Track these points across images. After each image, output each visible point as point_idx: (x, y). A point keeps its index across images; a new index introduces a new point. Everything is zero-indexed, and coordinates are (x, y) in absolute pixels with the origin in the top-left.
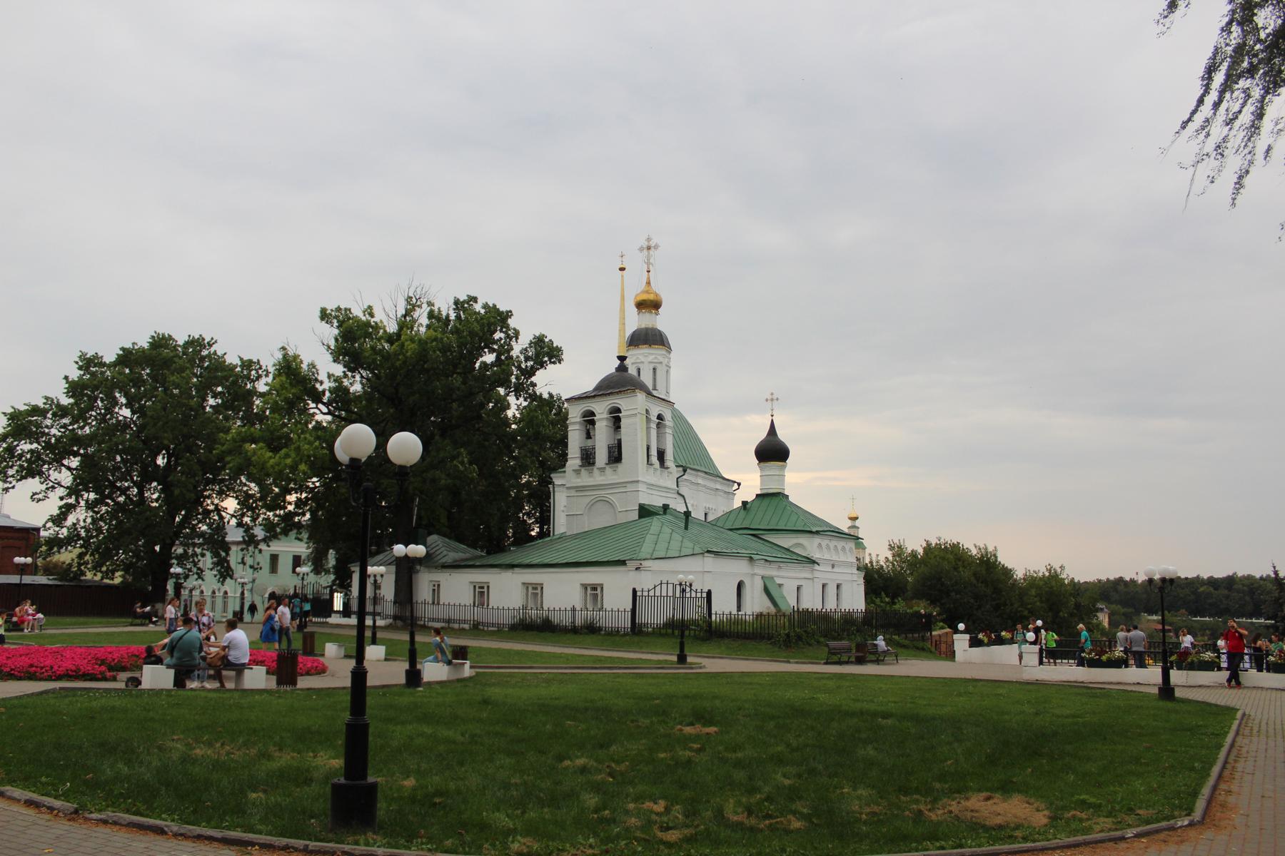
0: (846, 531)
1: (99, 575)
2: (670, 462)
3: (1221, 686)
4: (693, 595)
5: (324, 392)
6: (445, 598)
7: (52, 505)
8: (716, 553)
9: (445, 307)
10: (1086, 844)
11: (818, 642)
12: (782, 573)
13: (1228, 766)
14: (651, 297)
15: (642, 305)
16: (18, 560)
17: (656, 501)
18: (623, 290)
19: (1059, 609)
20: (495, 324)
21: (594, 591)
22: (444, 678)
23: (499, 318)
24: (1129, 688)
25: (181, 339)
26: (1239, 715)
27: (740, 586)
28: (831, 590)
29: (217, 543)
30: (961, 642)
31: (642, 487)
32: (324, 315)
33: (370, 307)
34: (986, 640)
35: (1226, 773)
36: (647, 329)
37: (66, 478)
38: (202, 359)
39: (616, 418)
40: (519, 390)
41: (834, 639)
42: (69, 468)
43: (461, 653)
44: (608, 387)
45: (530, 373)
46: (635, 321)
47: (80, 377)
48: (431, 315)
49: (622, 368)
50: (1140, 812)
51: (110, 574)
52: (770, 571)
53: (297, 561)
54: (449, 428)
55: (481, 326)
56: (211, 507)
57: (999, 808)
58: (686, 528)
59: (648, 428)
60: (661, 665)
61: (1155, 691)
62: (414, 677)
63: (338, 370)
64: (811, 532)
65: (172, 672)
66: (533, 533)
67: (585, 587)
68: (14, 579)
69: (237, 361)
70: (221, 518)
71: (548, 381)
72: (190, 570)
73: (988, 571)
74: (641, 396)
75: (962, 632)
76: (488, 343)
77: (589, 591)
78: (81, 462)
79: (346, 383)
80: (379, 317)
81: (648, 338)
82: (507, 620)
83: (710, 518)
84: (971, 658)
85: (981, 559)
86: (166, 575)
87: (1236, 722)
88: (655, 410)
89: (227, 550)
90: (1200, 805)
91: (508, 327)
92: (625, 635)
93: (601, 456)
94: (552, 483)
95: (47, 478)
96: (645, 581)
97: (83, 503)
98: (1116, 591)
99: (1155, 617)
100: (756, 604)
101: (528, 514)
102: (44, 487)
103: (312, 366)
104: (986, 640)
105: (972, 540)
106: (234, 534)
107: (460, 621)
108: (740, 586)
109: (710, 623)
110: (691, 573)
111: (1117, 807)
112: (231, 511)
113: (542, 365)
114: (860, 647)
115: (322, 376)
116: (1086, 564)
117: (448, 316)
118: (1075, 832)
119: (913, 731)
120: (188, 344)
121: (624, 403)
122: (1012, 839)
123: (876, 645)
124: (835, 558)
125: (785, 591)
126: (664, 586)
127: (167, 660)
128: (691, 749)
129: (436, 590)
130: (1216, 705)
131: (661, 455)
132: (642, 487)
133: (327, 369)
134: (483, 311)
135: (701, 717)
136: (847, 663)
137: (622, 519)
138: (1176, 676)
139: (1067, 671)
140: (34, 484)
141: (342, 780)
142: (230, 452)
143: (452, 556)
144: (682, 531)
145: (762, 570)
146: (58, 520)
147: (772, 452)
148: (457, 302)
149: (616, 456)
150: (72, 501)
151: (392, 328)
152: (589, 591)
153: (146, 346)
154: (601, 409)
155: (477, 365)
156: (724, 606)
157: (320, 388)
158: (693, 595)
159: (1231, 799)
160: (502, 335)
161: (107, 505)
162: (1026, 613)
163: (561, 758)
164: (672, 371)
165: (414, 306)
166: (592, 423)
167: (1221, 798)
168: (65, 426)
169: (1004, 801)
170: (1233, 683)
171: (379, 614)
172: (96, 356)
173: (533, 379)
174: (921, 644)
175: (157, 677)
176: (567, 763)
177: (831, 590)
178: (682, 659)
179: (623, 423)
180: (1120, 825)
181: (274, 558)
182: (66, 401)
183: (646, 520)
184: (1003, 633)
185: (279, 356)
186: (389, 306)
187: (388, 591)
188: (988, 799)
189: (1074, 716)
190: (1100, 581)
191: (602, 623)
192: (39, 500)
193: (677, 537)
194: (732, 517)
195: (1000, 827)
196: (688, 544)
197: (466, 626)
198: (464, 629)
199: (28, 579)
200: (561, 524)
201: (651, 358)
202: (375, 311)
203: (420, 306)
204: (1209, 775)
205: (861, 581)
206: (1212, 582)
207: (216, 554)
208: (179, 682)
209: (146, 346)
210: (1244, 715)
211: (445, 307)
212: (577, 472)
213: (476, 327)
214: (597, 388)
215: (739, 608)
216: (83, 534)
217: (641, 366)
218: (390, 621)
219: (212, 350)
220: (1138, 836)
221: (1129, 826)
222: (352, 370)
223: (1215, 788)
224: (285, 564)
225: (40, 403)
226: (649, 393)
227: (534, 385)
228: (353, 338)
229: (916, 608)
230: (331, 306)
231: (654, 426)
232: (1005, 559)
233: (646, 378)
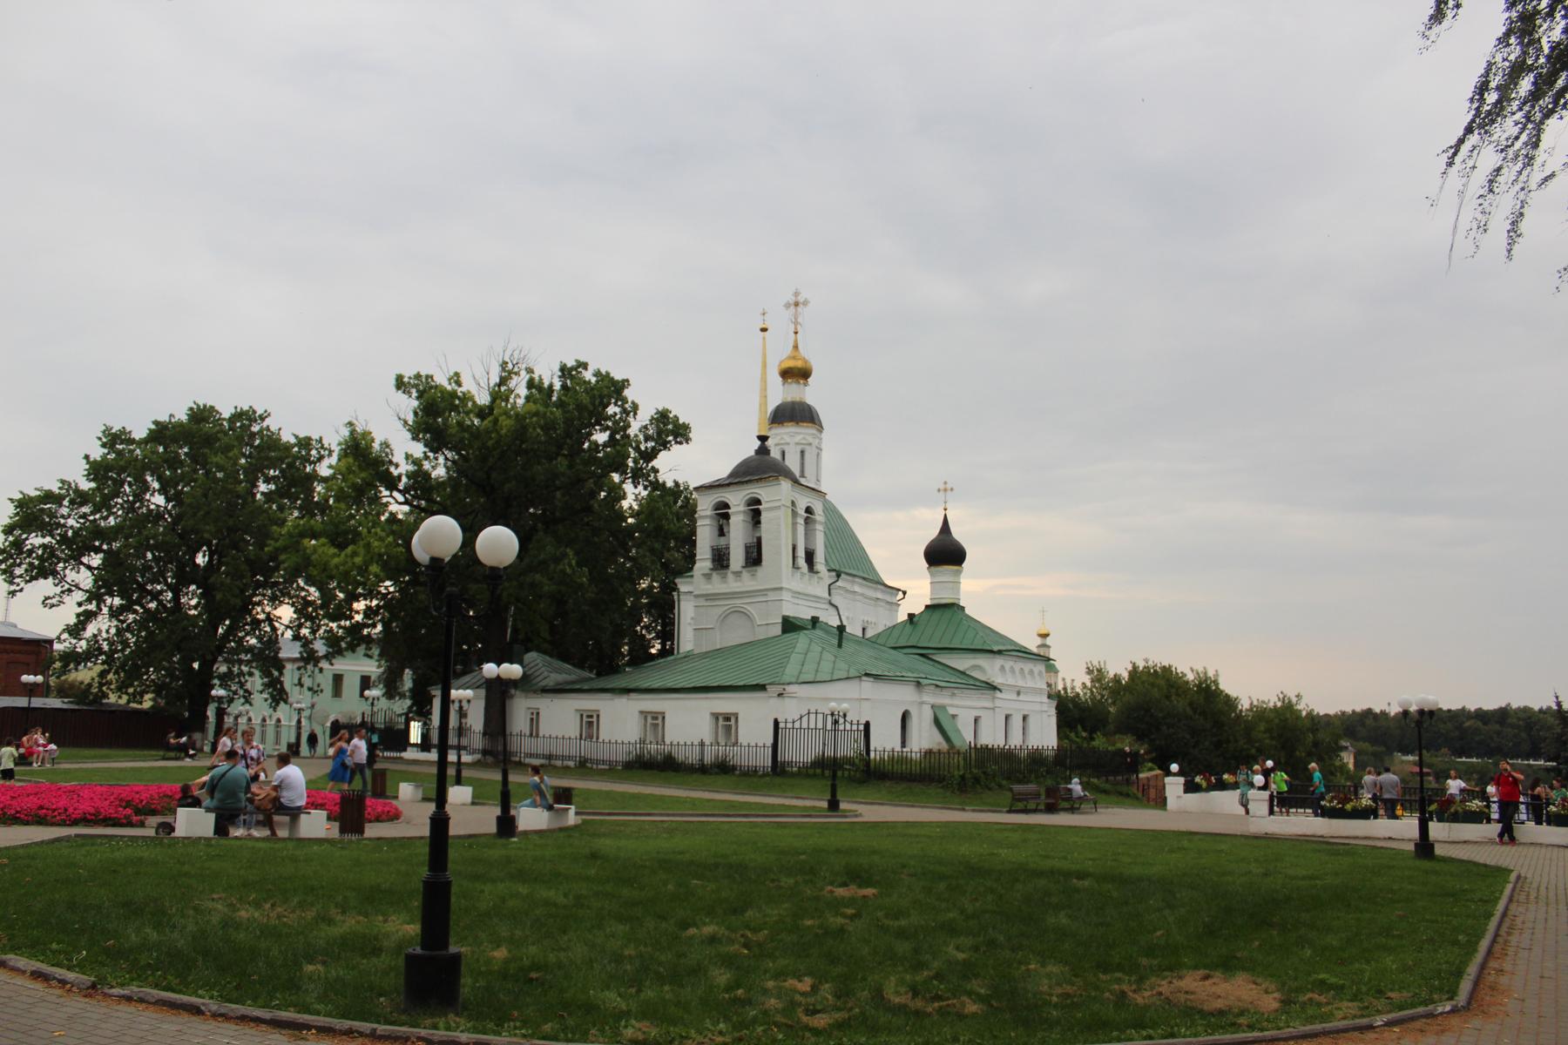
0: (1035, 650)
1: (125, 698)
3: (1491, 842)
4: (848, 727)
5: (400, 477)
6: (544, 729)
7: (69, 612)
8: (876, 677)
9: (549, 375)
10: (1325, 1033)
11: (1000, 786)
12: (956, 701)
13: (1500, 940)
14: (799, 364)
15: (787, 374)
16: (26, 678)
17: (803, 612)
18: (764, 355)
19: (1298, 750)
20: (610, 397)
21: (727, 722)
22: (544, 827)
23: (613, 388)
24: (1380, 844)
26: (1513, 877)
27: (905, 717)
28: (1016, 722)
29: (268, 659)
30: (1174, 786)
31: (786, 596)
33: (457, 374)
34: (1204, 784)
35: (1497, 947)
36: (793, 404)
37: (85, 579)
38: (253, 435)
39: (755, 516)
40: (637, 476)
41: (1020, 782)
42: (89, 567)
43: (564, 796)
44: (746, 473)
45: (650, 456)
46: (779, 393)
47: (104, 456)
49: (763, 451)
50: (1390, 994)
52: (943, 699)
53: (366, 683)
54: (551, 523)
55: (589, 399)
56: (262, 616)
57: (1219, 990)
58: (840, 645)
59: (794, 524)
60: (808, 812)
61: (1411, 847)
62: (506, 824)
63: (418, 449)
64: (991, 652)
65: (212, 817)
66: (653, 651)
67: (716, 716)
68: (21, 702)
69: (293, 441)
70: (274, 629)
71: (674, 466)
72: (235, 693)
73: (1207, 699)
74: (785, 485)
75: (1175, 775)
76: (599, 419)
77: (721, 722)
78: (104, 560)
79: (427, 466)
80: (468, 386)
81: (795, 414)
82: (621, 756)
83: (869, 634)
84: (1185, 806)
85: (1199, 686)
86: (207, 699)
87: (1509, 887)
89: (281, 668)
90: (1465, 986)
92: (764, 775)
93: (737, 557)
94: (675, 589)
95: (63, 579)
96: (788, 710)
97: (105, 610)
98: (1363, 725)
100: (923, 739)
101: (646, 627)
102: (58, 590)
103: (386, 445)
104: (1204, 784)
105: (1187, 664)
106: (289, 650)
107: (563, 758)
108: (905, 717)
109: (868, 763)
110: (844, 700)
111: (1364, 989)
112: (286, 622)
113: (665, 446)
114: (1050, 792)
115: (398, 457)
116: (1329, 689)
117: (551, 386)
118: (1311, 1020)
119: (1115, 894)
120: (239, 415)
121: (764, 492)
122: (1235, 1026)
123: (1070, 790)
124: (1021, 683)
125: (960, 724)
126: (812, 716)
127: (207, 802)
129: (535, 719)
130: (1486, 866)
131: (810, 557)
132: (786, 596)
133: (404, 450)
134: (593, 380)
135: (856, 876)
136: (1035, 811)
137: (761, 634)
138: (1437, 829)
139: (1303, 823)
140: (46, 586)
141: (419, 950)
142: (285, 549)
143: (554, 678)
144: (834, 650)
145: (930, 698)
146: (75, 630)
147: (945, 554)
148: (563, 369)
149: (754, 557)
150: (92, 607)
151: (483, 399)
152: (721, 722)
153: (184, 418)
154: (737, 499)
156: (885, 741)
157: (395, 472)
158: (848, 727)
159: (1504, 980)
160: (617, 410)
161: (135, 612)
162: (1253, 751)
163: (684, 925)
164: (825, 455)
165: (510, 372)
166: (726, 517)
167: (1491, 978)
168: (84, 516)
169: (1226, 980)
170: (1506, 838)
171: (465, 748)
172: (123, 431)
173: (655, 463)
174: (1124, 789)
175: (193, 822)
176: (692, 931)
177: (1016, 722)
178: (834, 805)
180: (1366, 1011)
181: (338, 679)
182: (86, 486)
183: (790, 636)
184: (1226, 776)
185: (346, 432)
186: (480, 372)
187: (476, 720)
188: (1206, 978)
189: (1311, 878)
190: (1343, 713)
191: (737, 761)
192: (53, 606)
193: (828, 656)
194: (896, 633)
195: (1221, 1013)
196: (841, 665)
197: (571, 764)
198: (568, 767)
199: (37, 702)
200: (687, 640)
201: (798, 438)
202: (463, 379)
204: (1475, 950)
205: (1053, 712)
206: (1481, 715)
207: (266, 673)
208: (221, 829)
209: (184, 418)
210: (1519, 877)
211: (549, 375)
212: (708, 576)
213: (585, 399)
214: (730, 476)
215: (903, 744)
216: (106, 647)
217: (786, 448)
218: (478, 756)
219: (265, 424)
220: (1389, 1024)
221: (1379, 1012)
222: (435, 451)
223: (1483, 966)
224: (351, 686)
225: (55, 487)
226: (796, 481)
227: (656, 471)
228: (436, 412)
229: (1119, 745)
230: (408, 373)
231: (801, 521)
232: (1228, 686)
233: (792, 463)
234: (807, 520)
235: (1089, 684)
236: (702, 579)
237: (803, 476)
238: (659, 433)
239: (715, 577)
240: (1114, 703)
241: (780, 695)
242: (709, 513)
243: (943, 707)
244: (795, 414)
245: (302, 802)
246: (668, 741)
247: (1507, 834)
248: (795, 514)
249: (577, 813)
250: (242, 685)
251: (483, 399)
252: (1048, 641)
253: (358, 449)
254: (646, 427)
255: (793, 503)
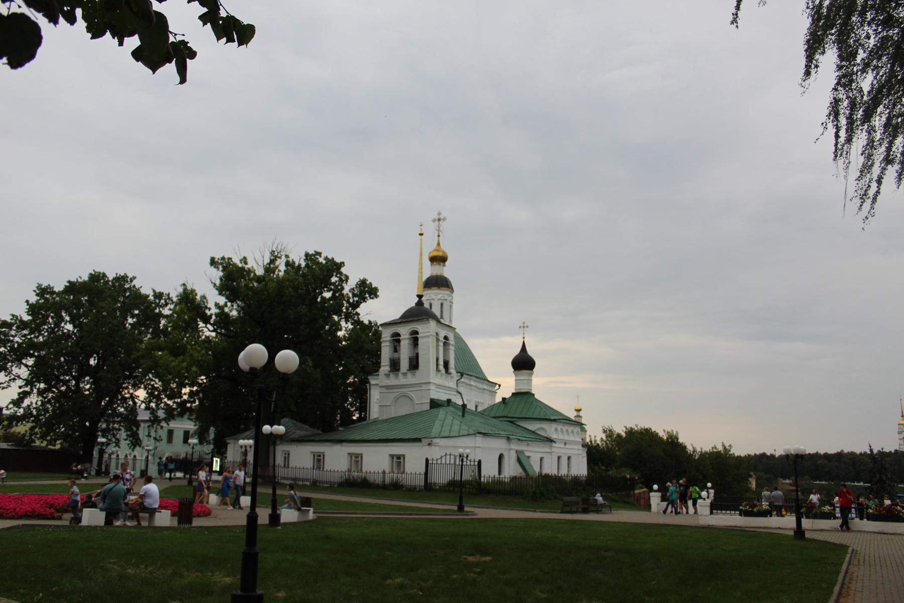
1: (45, 443)
2: (452, 370)
3: (836, 530)
4: (469, 463)
5: (211, 315)
6: (293, 463)
8: (485, 434)
9: (299, 259)
12: (530, 449)
13: (845, 586)
14: (440, 254)
17: (443, 396)
19: (728, 476)
21: (398, 460)
23: (335, 267)
25: (111, 276)
26: (850, 550)
27: (501, 457)
28: (564, 461)
29: (131, 421)
31: (432, 387)
32: (213, 262)
33: (245, 258)
35: (844, 591)
37: (24, 372)
38: (125, 290)
39: (415, 339)
40: (348, 317)
42: (26, 366)
43: (307, 502)
44: (410, 316)
45: (356, 305)
46: (429, 270)
48: (288, 264)
49: (420, 303)
51: (52, 442)
53: (187, 435)
55: (322, 271)
56: (128, 396)
58: (463, 416)
59: (438, 346)
61: (792, 533)
63: (222, 300)
64: (550, 420)
65: (104, 513)
66: (354, 418)
67: (392, 456)
70: (135, 403)
71: (369, 312)
72: (110, 440)
73: (673, 446)
74: (433, 323)
75: (656, 491)
77: (395, 460)
78: (36, 362)
81: (438, 282)
82: (336, 479)
87: (848, 556)
88: (443, 333)
89: (138, 426)
91: (341, 273)
92: (420, 491)
93: (404, 365)
94: (368, 382)
95: (10, 373)
97: (35, 391)
99: (788, 481)
100: (511, 470)
102: (7, 379)
103: (204, 297)
106: (143, 416)
107: (303, 480)
108: (501, 457)
112: (142, 398)
113: (364, 300)
115: (211, 304)
117: (300, 265)
124: (566, 438)
126: (448, 457)
127: (101, 505)
128: (474, 573)
130: (834, 544)
131: (446, 364)
132: (432, 387)
133: (214, 300)
134: (324, 262)
135: (481, 550)
136: (576, 512)
137: (418, 409)
138: (806, 523)
141: (239, 592)
145: (515, 446)
146: (17, 403)
147: (523, 363)
148: (307, 255)
149: (414, 364)
150: (28, 389)
151: (260, 272)
152: (395, 460)
153: (86, 279)
154: (404, 331)
155: (319, 300)
156: (489, 471)
157: (208, 312)
161: (53, 392)
164: (454, 306)
165: (276, 257)
166: (399, 341)
168: (25, 336)
170: (844, 528)
172: (49, 287)
173: (358, 310)
175: (92, 517)
176: (389, 581)
177: (564, 461)
178: (461, 508)
179: (420, 341)
181: (170, 433)
182: (26, 318)
183: (435, 410)
185: (181, 290)
186: (258, 256)
190: (749, 455)
191: (404, 482)
192: (4, 388)
193: (457, 422)
196: (464, 427)
197: (308, 483)
200: (375, 412)
201: (439, 296)
203: (280, 258)
204: (832, 592)
205: (585, 455)
208: (109, 522)
209: (86, 279)
210: (853, 550)
212: (387, 375)
214: (402, 317)
215: (500, 473)
216: (35, 412)
217: (433, 302)
224: (178, 437)
225: (8, 319)
227: (358, 314)
228: (233, 278)
229: (623, 474)
230: (218, 256)
231: (441, 344)
233: (436, 310)
234: (445, 344)
235: (604, 438)
236: (384, 377)
237: (442, 317)
238: (361, 292)
239: (392, 375)
240: (619, 450)
241: (429, 444)
242: (389, 339)
243: (522, 452)
244: (438, 282)
245: (157, 506)
246: (364, 471)
247: (845, 526)
248: (438, 340)
249: (314, 513)
250: (114, 436)
251: (260, 272)
252: (581, 413)
253: (188, 298)
254: (353, 289)
255: (437, 334)
